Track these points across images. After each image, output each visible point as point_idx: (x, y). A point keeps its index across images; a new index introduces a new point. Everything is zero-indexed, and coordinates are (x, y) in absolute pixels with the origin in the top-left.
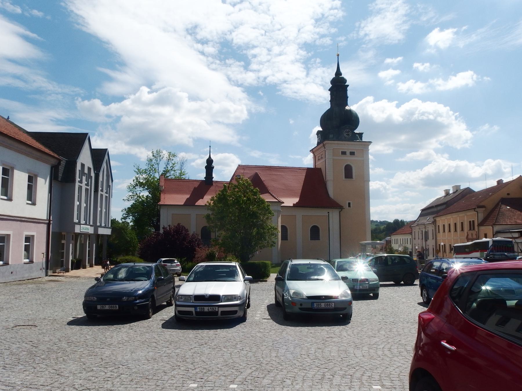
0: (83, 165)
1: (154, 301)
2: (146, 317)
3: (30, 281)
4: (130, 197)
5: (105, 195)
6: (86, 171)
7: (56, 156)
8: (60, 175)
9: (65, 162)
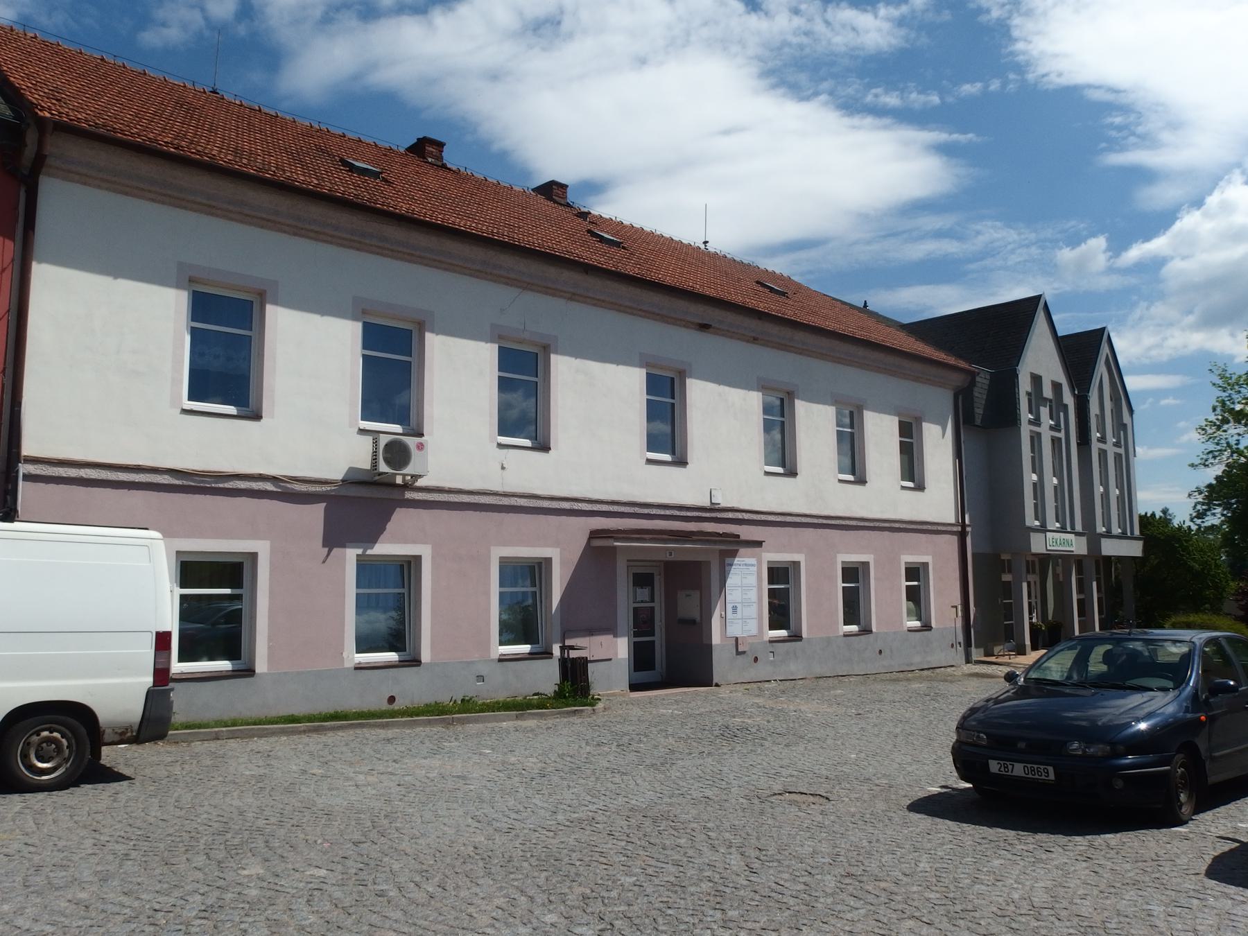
0: (1036, 380)
1: (1195, 763)
2: (1166, 817)
3: (926, 672)
4: (1210, 456)
5: (1111, 450)
6: (1048, 392)
7: (962, 364)
8: (979, 411)
9: (988, 377)
